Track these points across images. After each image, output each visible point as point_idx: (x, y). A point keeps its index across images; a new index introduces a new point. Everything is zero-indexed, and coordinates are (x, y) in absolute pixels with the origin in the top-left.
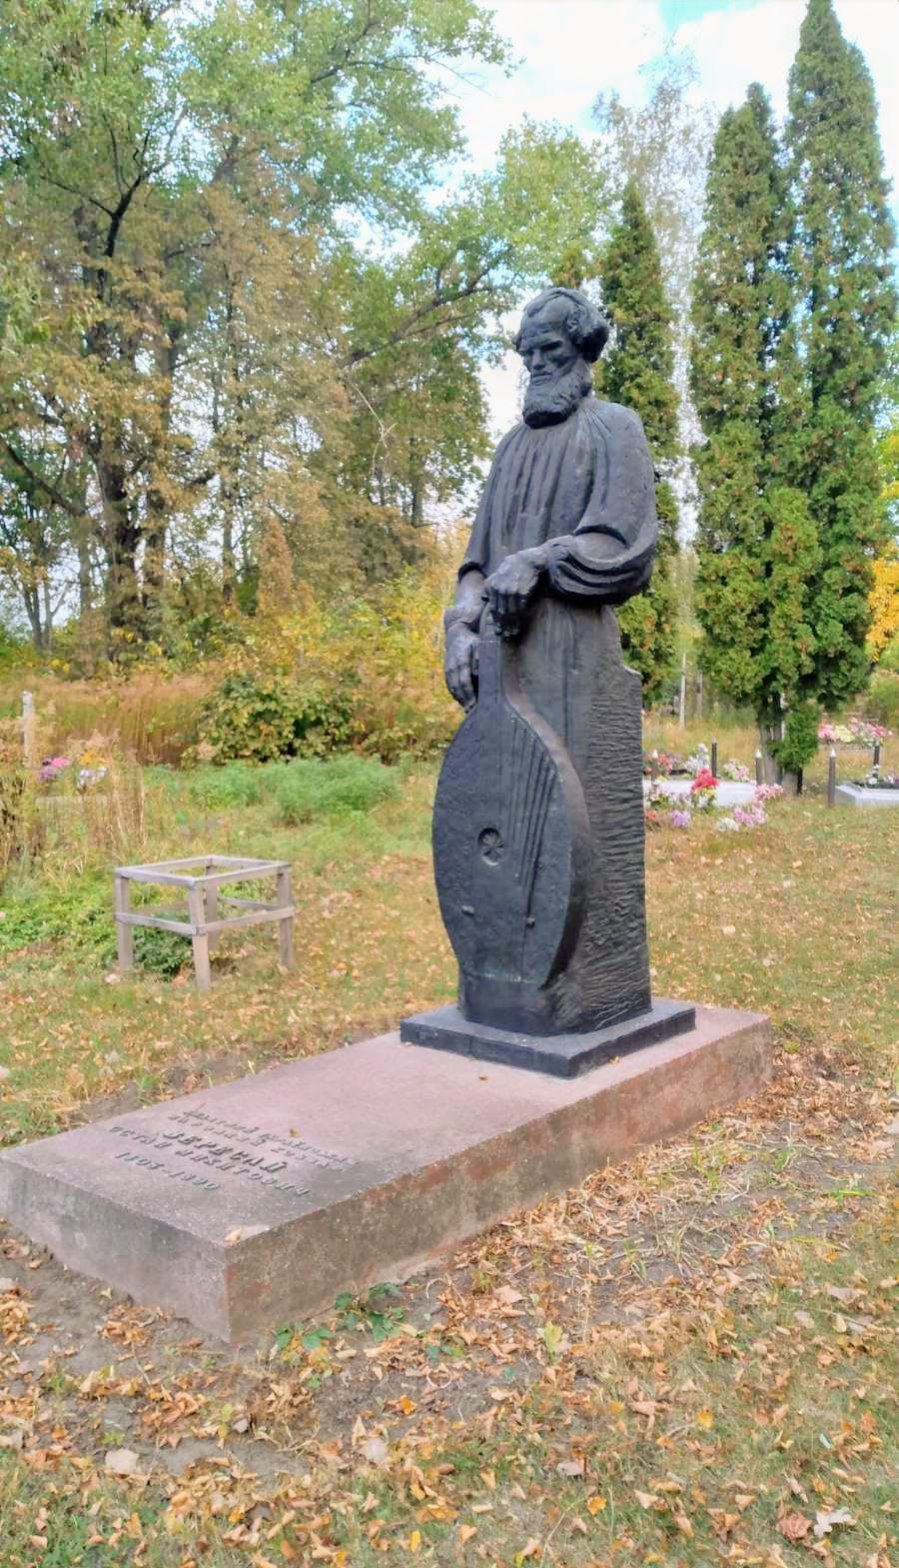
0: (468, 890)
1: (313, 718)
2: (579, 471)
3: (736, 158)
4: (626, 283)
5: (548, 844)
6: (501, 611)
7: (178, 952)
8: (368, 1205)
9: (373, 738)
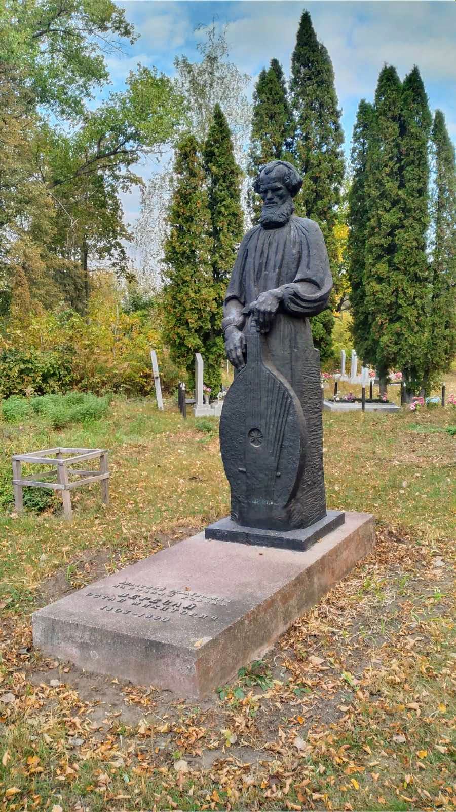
0: (241, 460)
1: (52, 372)
2: (294, 251)
3: (268, 96)
4: (218, 154)
5: (288, 435)
6: (261, 320)
7: (44, 499)
8: (246, 622)
9: (85, 382)
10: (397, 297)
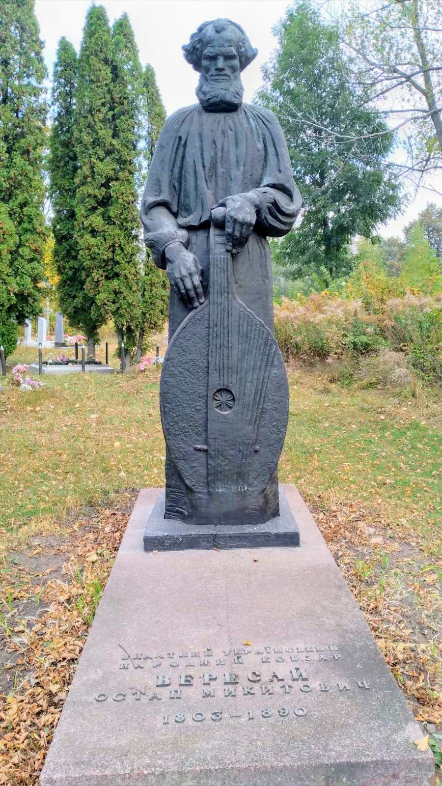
6: (237, 234)
10: (113, 252)
